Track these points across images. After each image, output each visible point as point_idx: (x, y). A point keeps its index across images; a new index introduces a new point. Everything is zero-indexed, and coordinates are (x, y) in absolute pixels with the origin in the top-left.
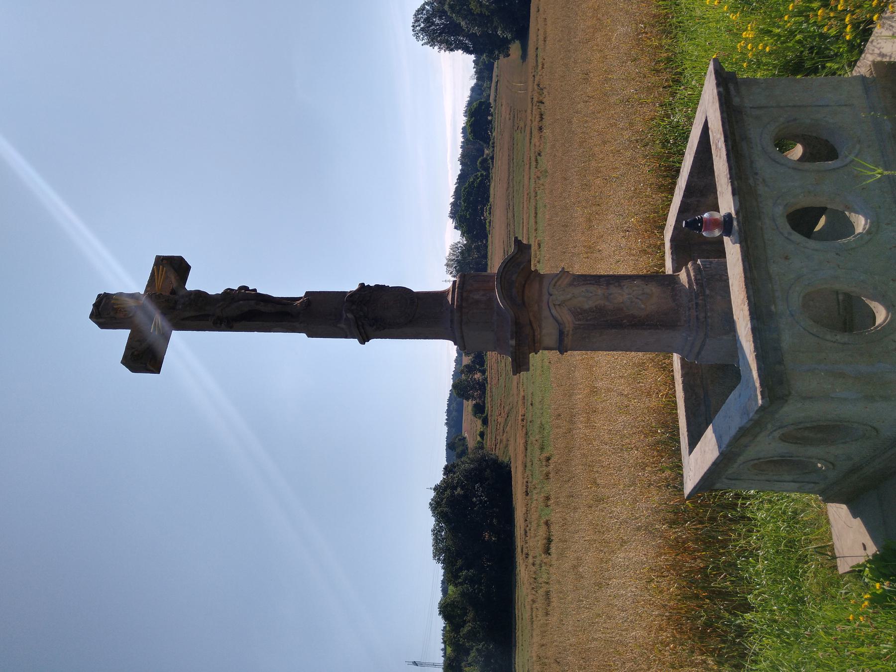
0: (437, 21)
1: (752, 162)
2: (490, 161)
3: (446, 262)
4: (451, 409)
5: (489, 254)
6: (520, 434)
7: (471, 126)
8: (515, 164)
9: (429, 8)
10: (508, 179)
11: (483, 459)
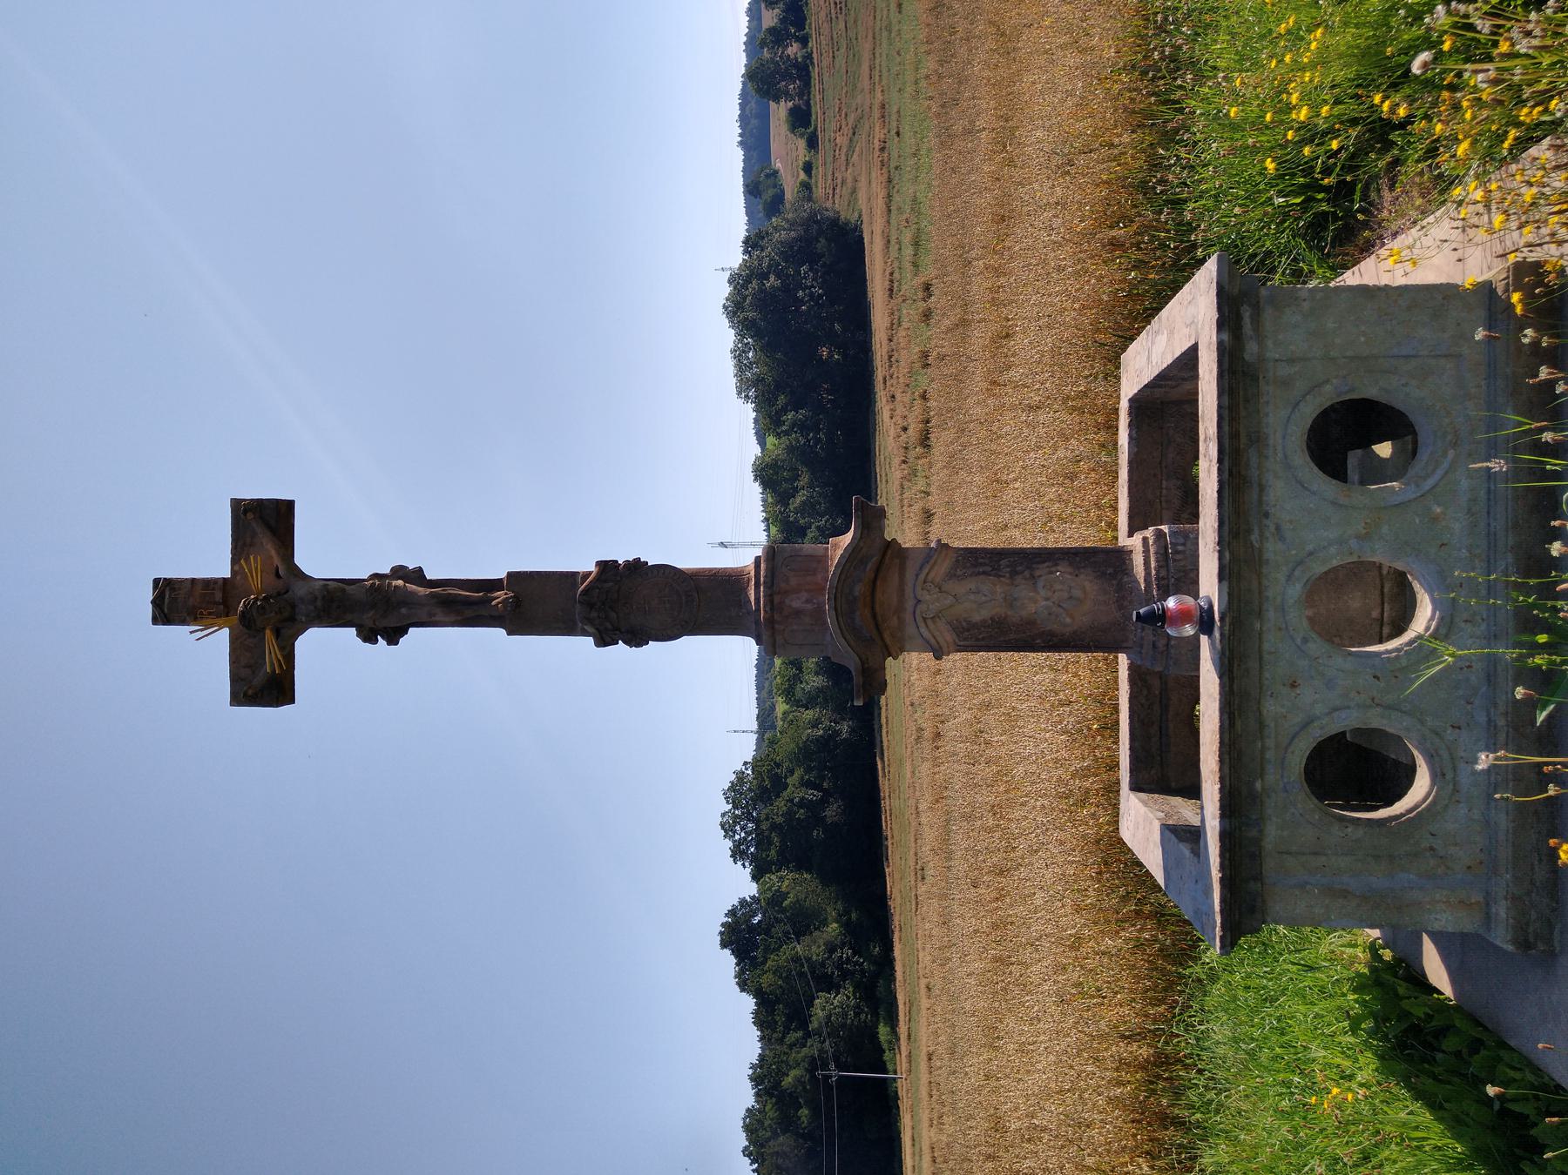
1: (1262, 489)
4: (747, 112)
6: (877, 177)
11: (812, 219)
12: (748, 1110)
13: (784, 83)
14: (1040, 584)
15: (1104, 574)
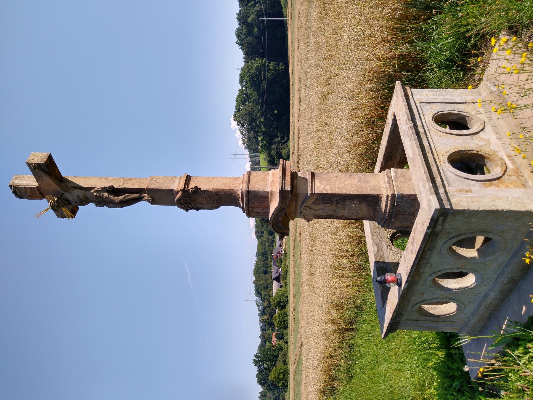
12: (237, 29)
14: (346, 209)
15: (370, 205)
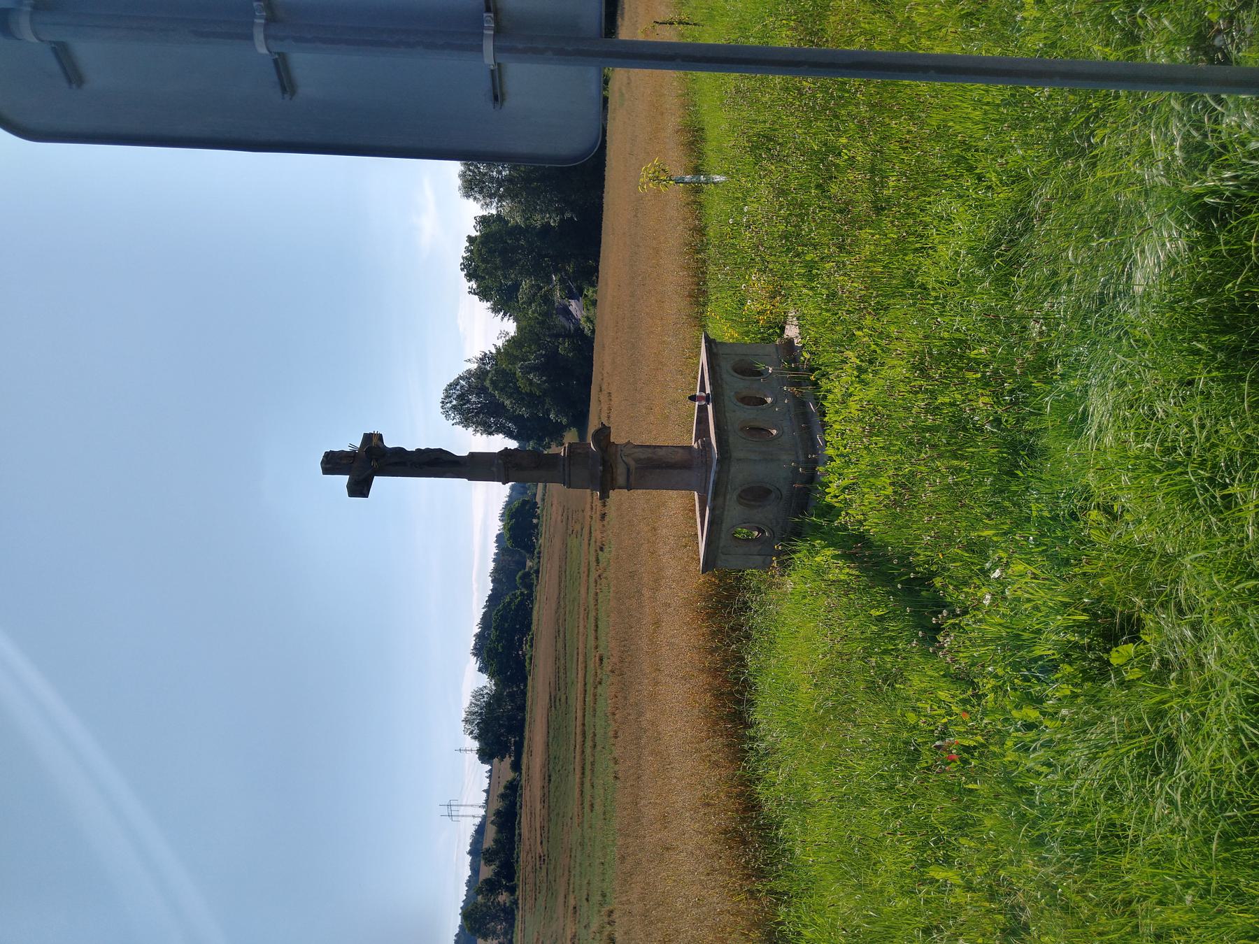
0: (473, 398)
2: (534, 576)
3: (464, 715)
5: (528, 703)
7: (509, 530)
8: (568, 577)
9: (464, 383)
10: (559, 598)
13: (493, 924)
